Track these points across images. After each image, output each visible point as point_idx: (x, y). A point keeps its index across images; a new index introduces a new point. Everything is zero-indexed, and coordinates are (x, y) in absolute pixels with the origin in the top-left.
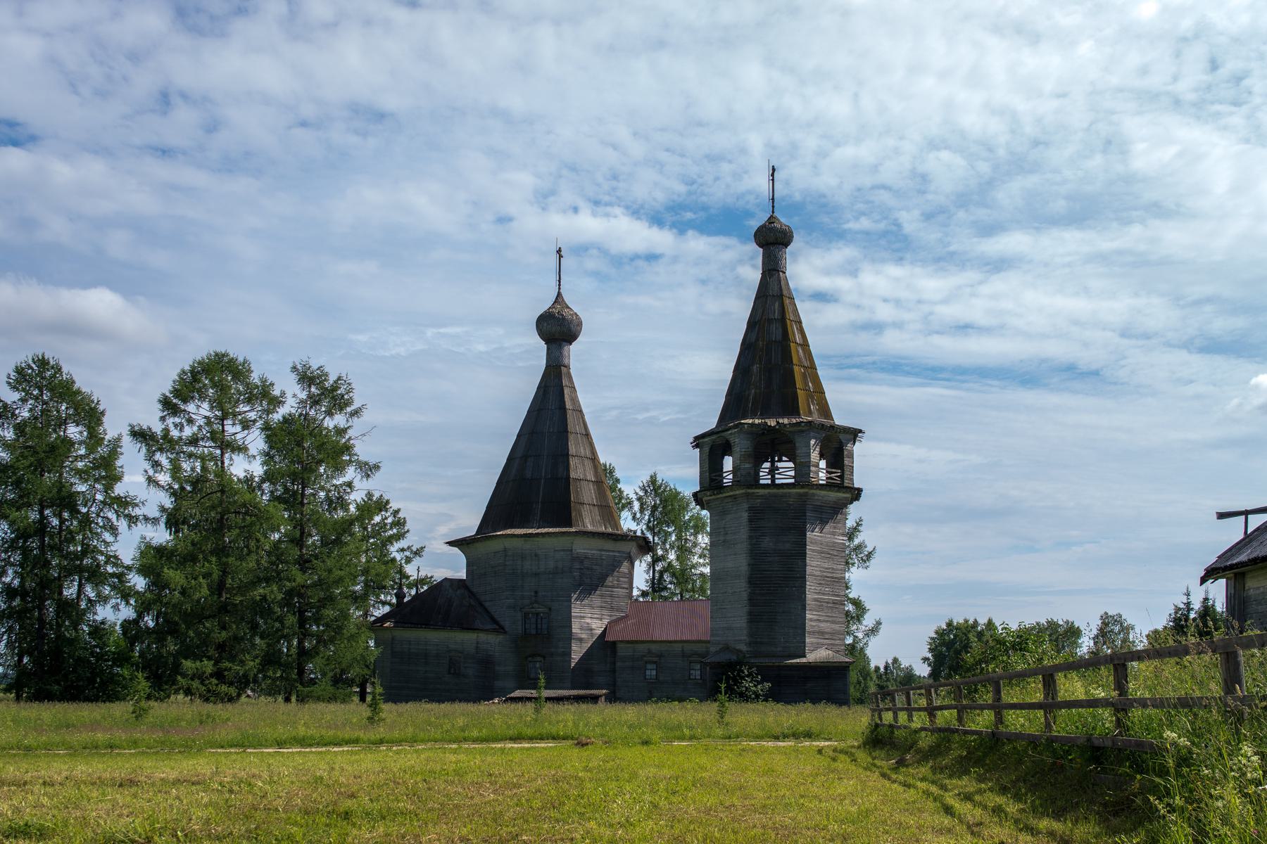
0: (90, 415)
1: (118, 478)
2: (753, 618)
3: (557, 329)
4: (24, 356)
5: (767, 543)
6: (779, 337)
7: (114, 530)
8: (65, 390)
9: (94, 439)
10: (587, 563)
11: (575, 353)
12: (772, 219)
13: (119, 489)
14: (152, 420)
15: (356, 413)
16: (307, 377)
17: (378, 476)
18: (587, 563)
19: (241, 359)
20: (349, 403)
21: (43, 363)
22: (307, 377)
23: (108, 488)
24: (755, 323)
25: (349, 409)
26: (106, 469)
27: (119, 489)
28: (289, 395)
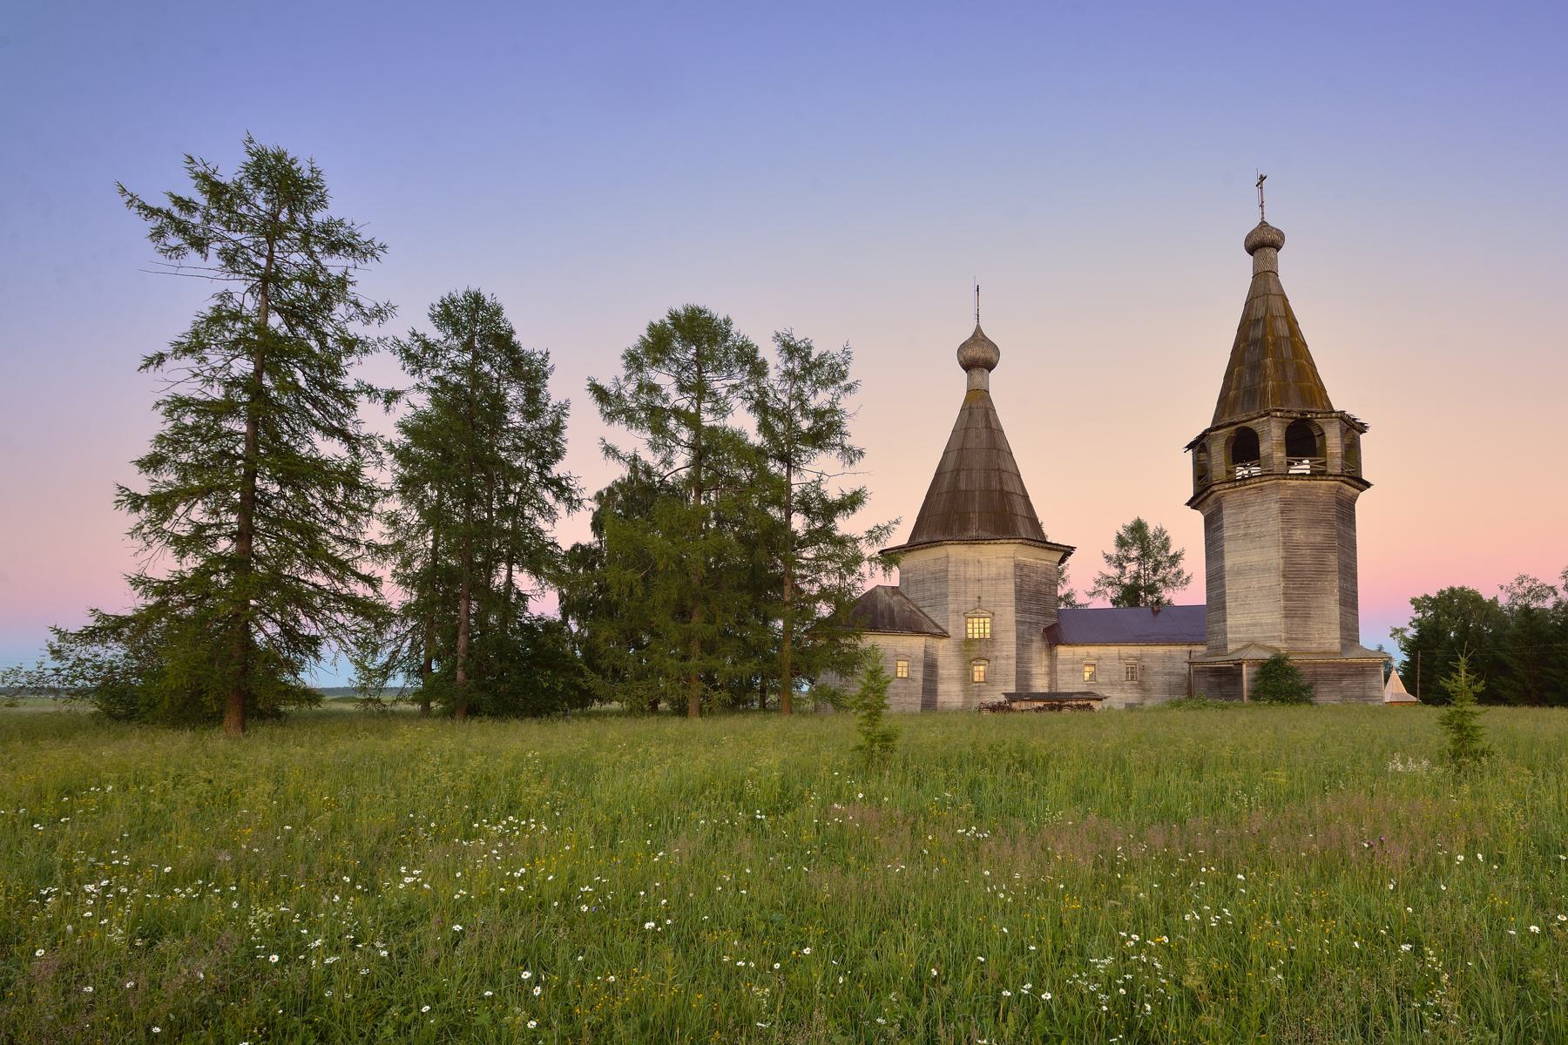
0: (529, 373)
1: (558, 455)
2: (1289, 614)
3: (978, 359)
4: (458, 286)
5: (1299, 535)
6: (1287, 334)
7: (549, 513)
8: (504, 342)
9: (533, 405)
10: (1026, 571)
11: (998, 383)
12: (1263, 224)
13: (557, 470)
14: (612, 373)
15: (849, 388)
16: (790, 349)
17: (860, 464)
18: (1026, 571)
19: (721, 317)
20: (843, 376)
21: (477, 301)
22: (790, 349)
23: (544, 467)
24: (1248, 323)
25: (842, 384)
26: (546, 446)
27: (557, 470)
28: (771, 366)
